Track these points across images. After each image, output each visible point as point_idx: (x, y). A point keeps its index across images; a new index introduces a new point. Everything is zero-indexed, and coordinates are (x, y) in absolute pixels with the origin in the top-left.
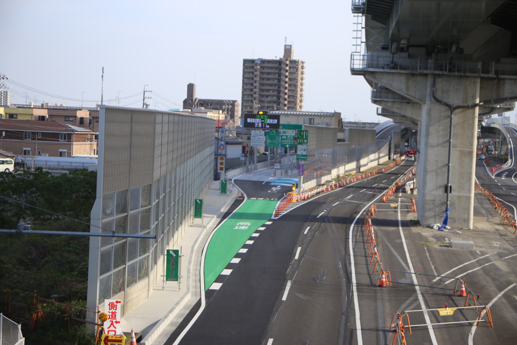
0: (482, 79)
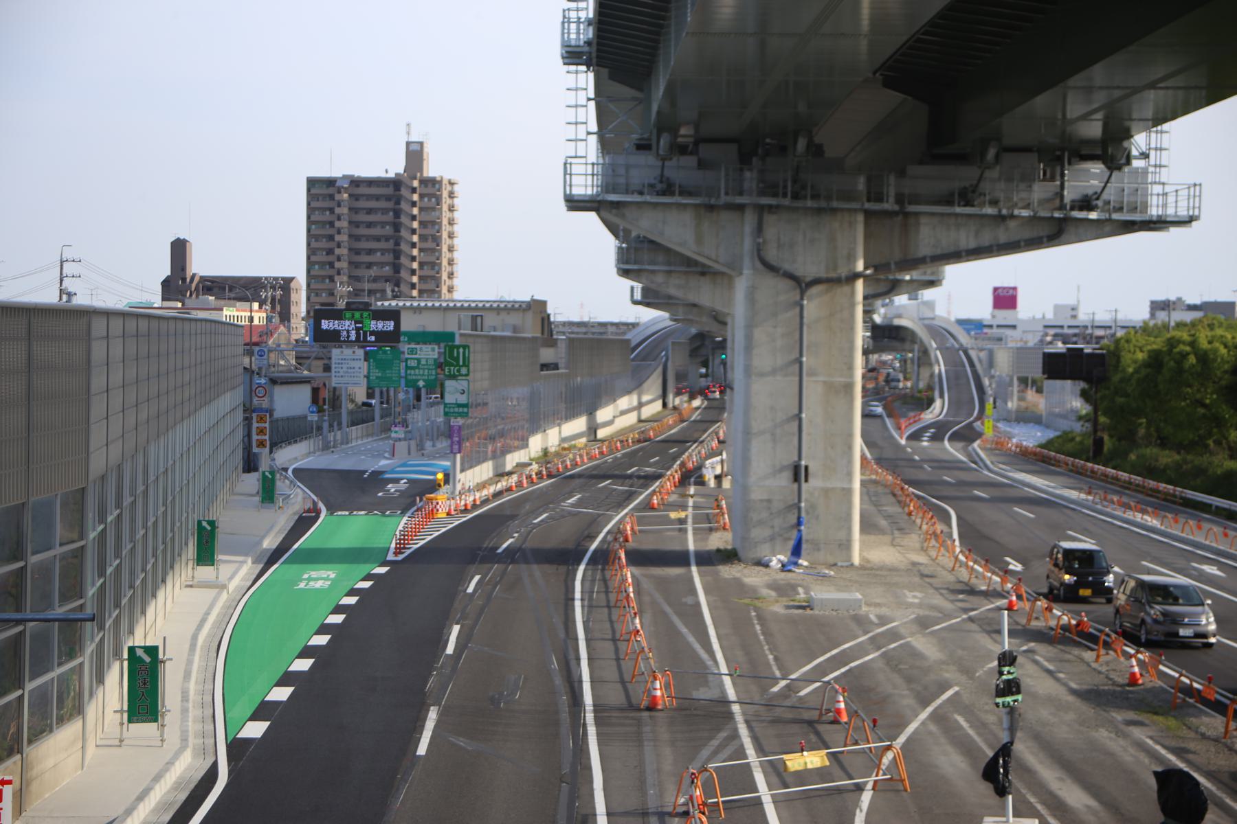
0: (868, 214)
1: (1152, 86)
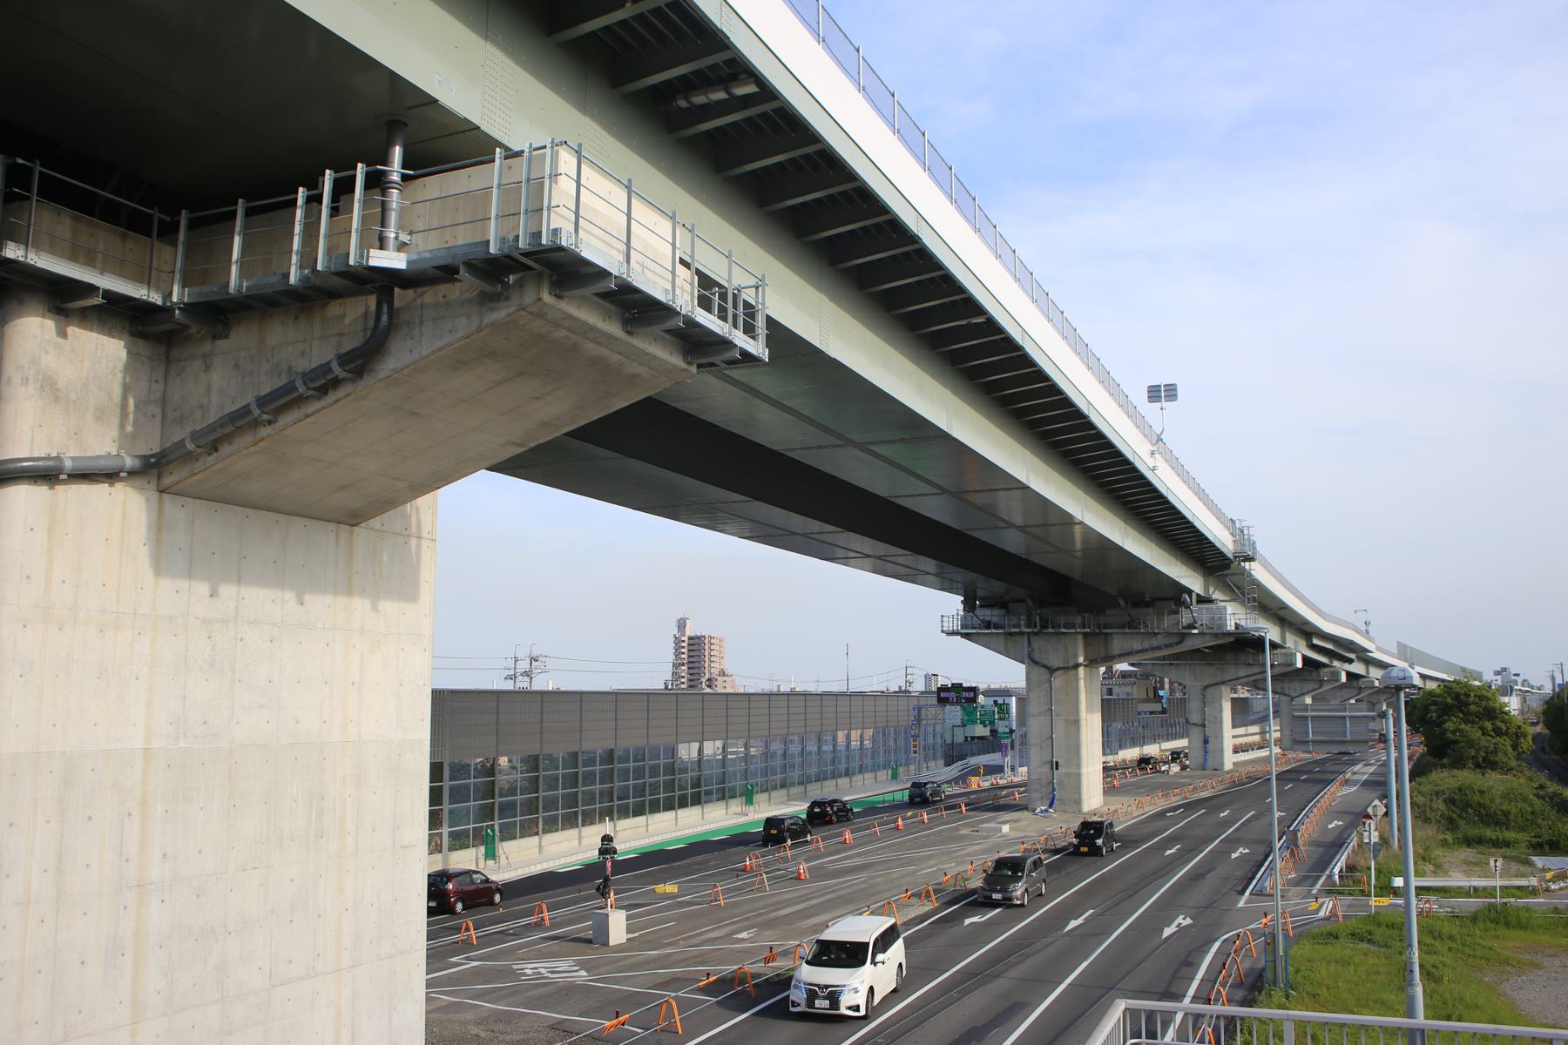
0: (1085, 635)
1: (119, 314)
